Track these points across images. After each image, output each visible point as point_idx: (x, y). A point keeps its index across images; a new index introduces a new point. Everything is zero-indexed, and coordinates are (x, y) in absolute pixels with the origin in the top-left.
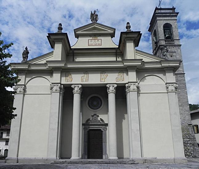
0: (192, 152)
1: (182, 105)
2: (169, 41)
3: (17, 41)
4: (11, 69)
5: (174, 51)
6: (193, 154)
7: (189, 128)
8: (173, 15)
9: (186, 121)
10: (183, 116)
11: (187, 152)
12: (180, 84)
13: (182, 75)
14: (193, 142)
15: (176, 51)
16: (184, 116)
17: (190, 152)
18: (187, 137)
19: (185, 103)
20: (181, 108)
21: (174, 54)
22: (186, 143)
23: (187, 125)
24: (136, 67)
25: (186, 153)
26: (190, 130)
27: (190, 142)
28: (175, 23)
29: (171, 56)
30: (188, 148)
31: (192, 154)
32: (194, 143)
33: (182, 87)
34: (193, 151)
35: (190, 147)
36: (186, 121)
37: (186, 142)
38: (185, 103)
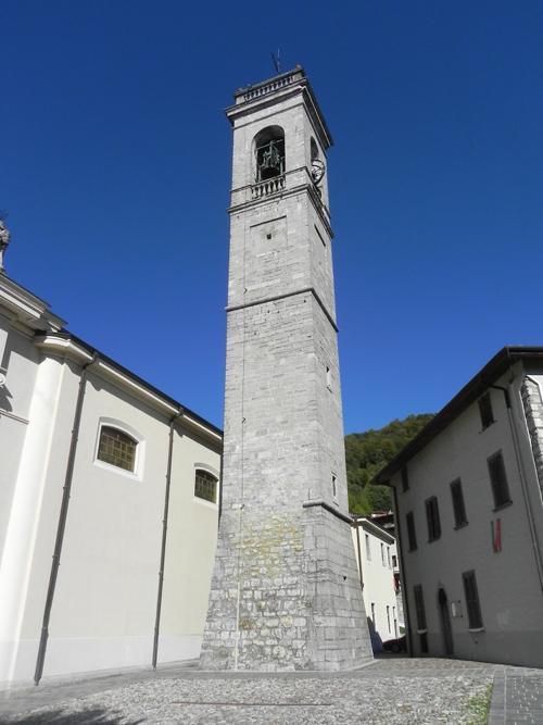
0: (299, 644)
1: (286, 422)
2: (262, 188)
3: (31, 334)
4: (398, 445)
5: (278, 216)
6: (299, 653)
7: (304, 521)
8: (286, 92)
9: (293, 493)
10: (285, 469)
11: (276, 642)
12: (289, 334)
13: (300, 295)
14: (313, 593)
15: (286, 213)
16: (290, 471)
17: (289, 643)
18: (287, 566)
19: (299, 410)
20: (281, 434)
21: (279, 226)
22: (279, 598)
23: (299, 509)
24: (15, 314)
25: (273, 646)
26: (308, 532)
27: (295, 593)
28: (293, 116)
29: (269, 237)
30: (283, 620)
31: (295, 651)
32: (316, 595)
33: (294, 346)
34: (306, 636)
35: (294, 616)
36: (293, 493)
37: (282, 593)
38: (299, 410)
